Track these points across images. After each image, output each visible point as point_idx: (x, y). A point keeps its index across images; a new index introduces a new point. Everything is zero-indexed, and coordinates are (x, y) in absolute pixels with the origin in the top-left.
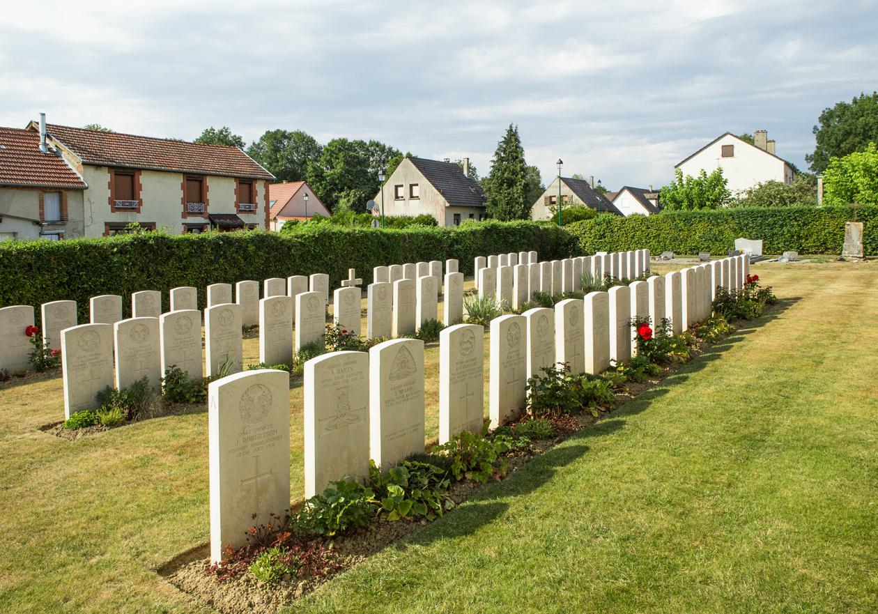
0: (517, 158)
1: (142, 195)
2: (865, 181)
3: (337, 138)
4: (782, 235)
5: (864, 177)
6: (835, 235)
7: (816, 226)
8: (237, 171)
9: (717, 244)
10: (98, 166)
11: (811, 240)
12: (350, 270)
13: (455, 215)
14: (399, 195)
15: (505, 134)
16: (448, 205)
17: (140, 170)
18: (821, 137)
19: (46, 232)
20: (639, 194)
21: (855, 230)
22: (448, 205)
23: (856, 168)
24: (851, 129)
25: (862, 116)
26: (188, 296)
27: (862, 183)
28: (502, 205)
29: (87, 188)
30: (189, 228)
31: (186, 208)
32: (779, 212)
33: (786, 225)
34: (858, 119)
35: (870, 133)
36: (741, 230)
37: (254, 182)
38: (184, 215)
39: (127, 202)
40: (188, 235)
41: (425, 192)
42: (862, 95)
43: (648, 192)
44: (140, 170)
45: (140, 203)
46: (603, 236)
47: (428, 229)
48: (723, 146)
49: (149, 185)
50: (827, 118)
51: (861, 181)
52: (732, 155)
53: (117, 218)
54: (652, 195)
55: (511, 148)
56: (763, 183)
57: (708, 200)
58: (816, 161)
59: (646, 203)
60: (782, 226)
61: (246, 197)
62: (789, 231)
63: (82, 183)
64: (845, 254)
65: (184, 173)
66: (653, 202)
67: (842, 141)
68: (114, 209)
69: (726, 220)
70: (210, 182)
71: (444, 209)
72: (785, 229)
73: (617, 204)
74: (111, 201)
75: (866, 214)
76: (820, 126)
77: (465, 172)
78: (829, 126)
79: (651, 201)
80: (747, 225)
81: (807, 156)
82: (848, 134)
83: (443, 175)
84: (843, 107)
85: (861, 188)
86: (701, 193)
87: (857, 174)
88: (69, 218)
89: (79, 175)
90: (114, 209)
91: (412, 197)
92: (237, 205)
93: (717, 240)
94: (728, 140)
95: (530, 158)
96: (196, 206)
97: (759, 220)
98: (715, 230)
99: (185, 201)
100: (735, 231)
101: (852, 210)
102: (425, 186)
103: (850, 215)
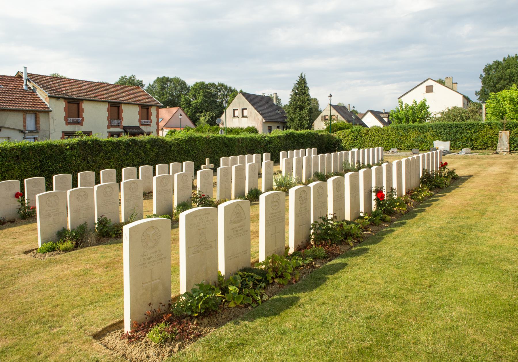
0: (305, 93)
1: (84, 115)
2: (511, 106)
3: (199, 81)
4: (462, 138)
5: (510, 104)
6: (493, 138)
7: (481, 133)
8: (140, 101)
9: (423, 144)
10: (58, 98)
11: (478, 142)
12: (207, 159)
13: (268, 127)
14: (236, 115)
15: (298, 79)
16: (264, 121)
17: (82, 100)
18: (485, 81)
19: (27, 137)
20: (377, 114)
21: (504, 136)
22: (264, 121)
23: (505, 99)
24: (502, 76)
25: (509, 68)
26: (111, 175)
27: (509, 108)
28: (296, 121)
29: (51, 111)
30: (112, 134)
31: (109, 122)
32: (460, 125)
33: (464, 133)
34: (506, 70)
35: (513, 79)
36: (437, 135)
37: (80, 102)
38: (109, 127)
39: (75, 119)
40: (111, 139)
41: (251, 113)
42: (509, 56)
43: (382, 113)
44: (82, 100)
45: (83, 120)
46: (356, 139)
47: (253, 135)
48: (427, 86)
49: (87, 108)
50: (488, 69)
51: (508, 106)
52: (432, 91)
53: (69, 128)
54: (385, 115)
55: (301, 88)
56: (450, 108)
57: (418, 118)
58: (482, 95)
59: (381, 120)
60: (461, 133)
61: (145, 116)
62: (465, 136)
63: (48, 108)
64: (499, 149)
65: (109, 102)
66: (386, 119)
67: (497, 83)
68: (68, 123)
69: (429, 130)
70: (124, 107)
71: (262, 123)
72: (463, 135)
73: (364, 120)
74: (66, 119)
75: (511, 126)
76: (484, 74)
77: (275, 102)
78: (489, 74)
79: (384, 119)
80: (441, 133)
81: (476, 92)
82: (500, 79)
83: (262, 103)
84: (497, 63)
85: (508, 111)
86: (414, 114)
87: (506, 103)
88: (41, 128)
89: (46, 103)
90: (68, 123)
91: (243, 116)
92: (140, 121)
93: (423, 142)
94: (430, 83)
95: (313, 93)
96: (116, 122)
97: (448, 130)
98: (422, 136)
99: (110, 118)
100: (433, 136)
101: (503, 124)
102: (251, 110)
103: (502, 127)
